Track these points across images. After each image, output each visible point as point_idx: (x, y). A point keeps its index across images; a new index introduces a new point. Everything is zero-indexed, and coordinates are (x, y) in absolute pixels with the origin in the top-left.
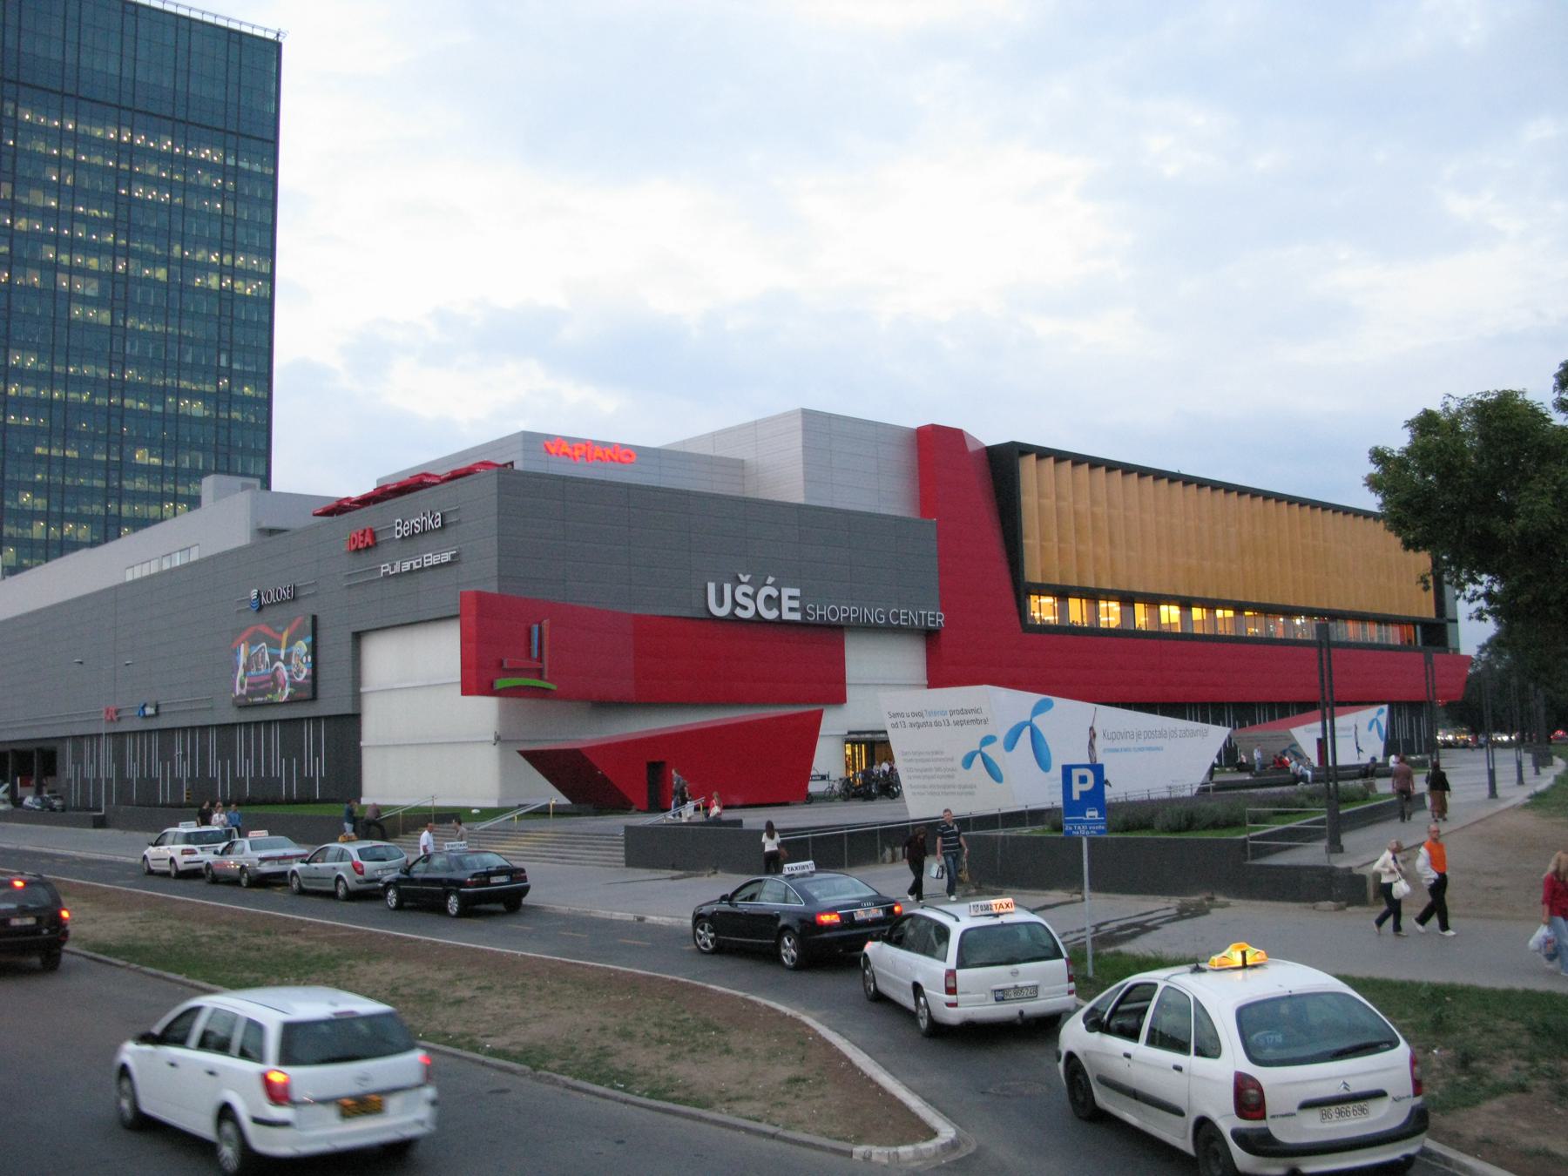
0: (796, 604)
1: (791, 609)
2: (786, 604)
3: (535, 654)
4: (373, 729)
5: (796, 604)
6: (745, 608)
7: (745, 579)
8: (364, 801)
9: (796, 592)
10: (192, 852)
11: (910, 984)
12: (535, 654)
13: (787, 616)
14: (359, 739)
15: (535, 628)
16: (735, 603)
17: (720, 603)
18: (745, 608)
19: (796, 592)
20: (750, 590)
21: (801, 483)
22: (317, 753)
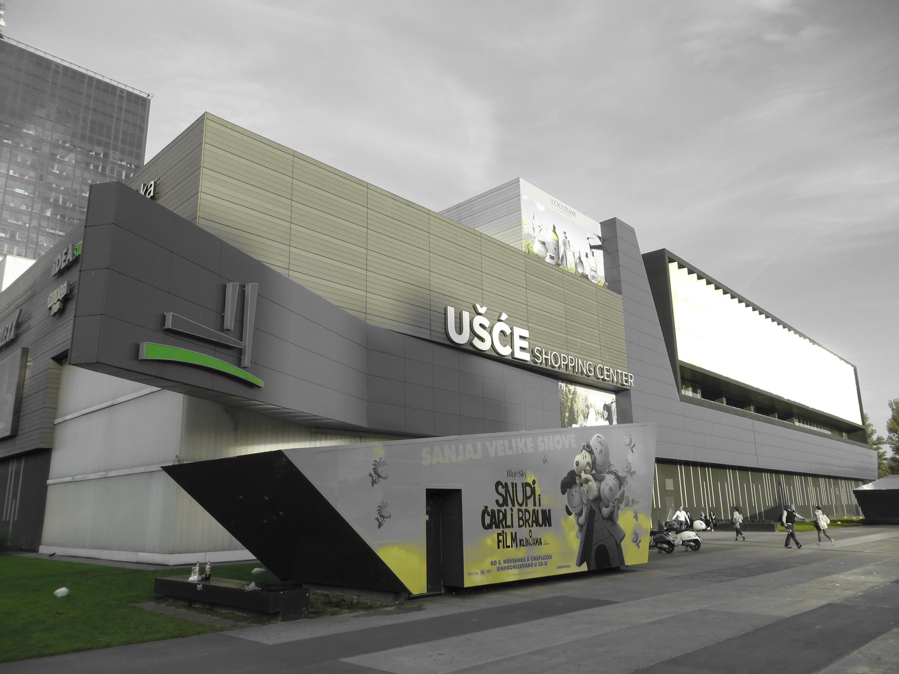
0: (525, 344)
1: (522, 349)
2: (518, 343)
3: (230, 321)
4: (61, 465)
5: (525, 344)
6: (482, 340)
7: (482, 310)
8: (44, 550)
9: (526, 333)
10: (636, 541)
11: (51, 361)
12: (230, 321)
13: (519, 355)
14: (46, 475)
15: (232, 292)
16: (473, 333)
17: (460, 330)
18: (482, 340)
19: (526, 333)
20: (487, 323)
21: (522, 208)
22: (14, 497)
